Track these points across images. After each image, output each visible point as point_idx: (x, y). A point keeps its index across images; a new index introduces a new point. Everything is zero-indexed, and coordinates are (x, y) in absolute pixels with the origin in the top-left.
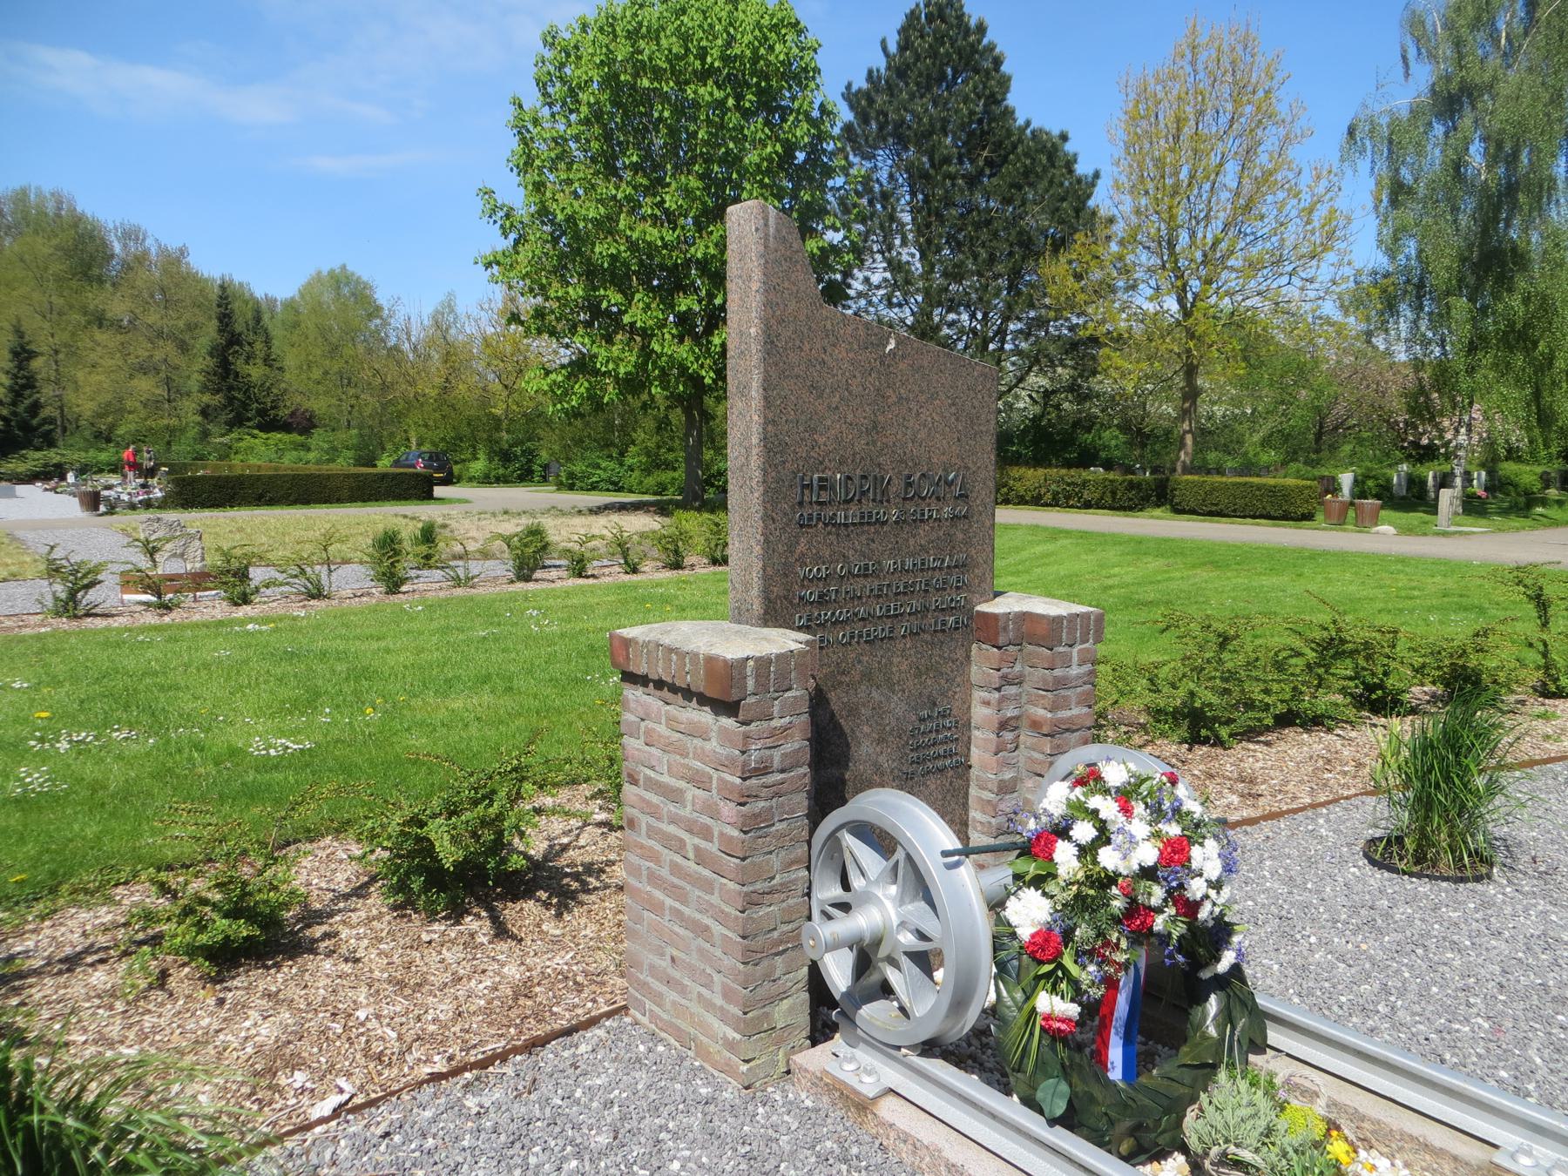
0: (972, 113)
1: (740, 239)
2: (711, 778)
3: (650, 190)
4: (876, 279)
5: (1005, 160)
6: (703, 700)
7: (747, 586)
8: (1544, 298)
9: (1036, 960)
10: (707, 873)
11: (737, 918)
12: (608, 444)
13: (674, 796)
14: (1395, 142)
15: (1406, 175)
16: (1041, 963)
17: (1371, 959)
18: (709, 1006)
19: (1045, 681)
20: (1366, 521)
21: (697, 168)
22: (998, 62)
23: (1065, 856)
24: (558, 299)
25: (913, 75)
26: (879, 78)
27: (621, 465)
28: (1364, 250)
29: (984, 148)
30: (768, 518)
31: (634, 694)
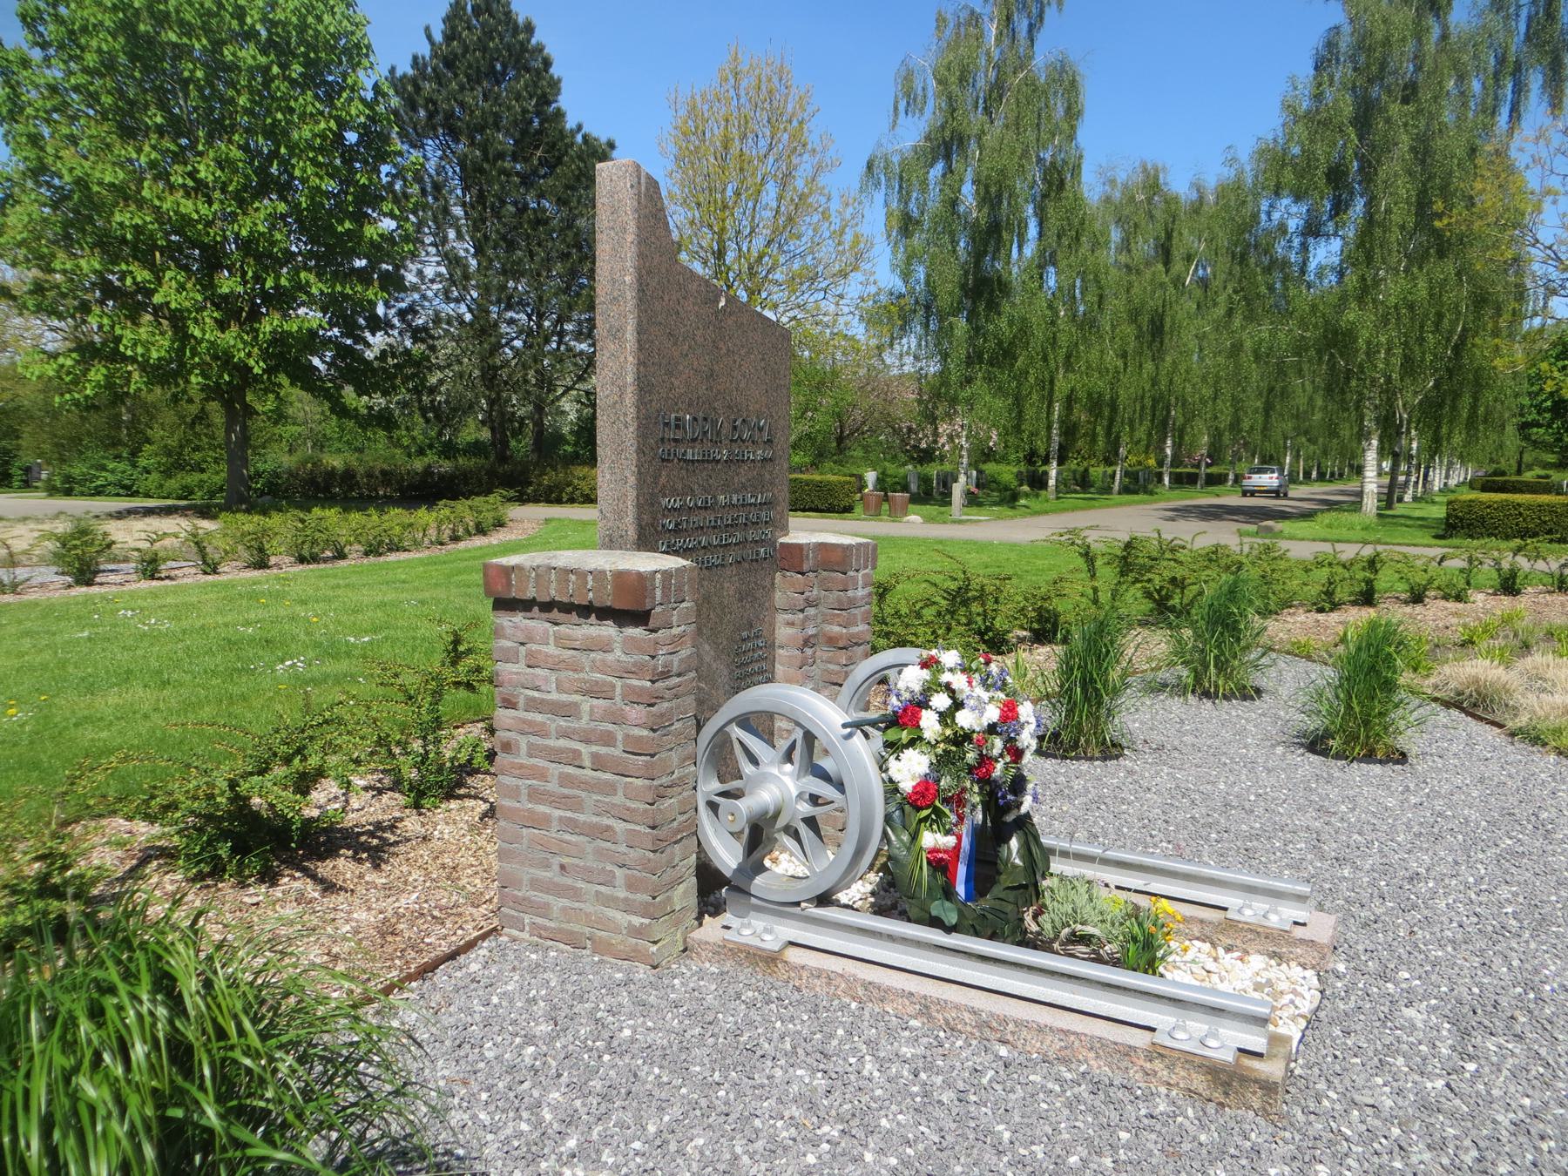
0: (525, 111)
1: (611, 194)
2: (614, 686)
3: (179, 157)
4: (429, 272)
5: (559, 161)
6: (605, 613)
7: (620, 515)
8: (1023, 319)
9: (918, 805)
10: (608, 776)
11: (646, 811)
12: (116, 443)
13: (568, 711)
14: (904, 180)
15: (913, 207)
16: (919, 809)
17: (1072, 815)
18: (609, 901)
19: (839, 600)
20: (897, 513)
21: (236, 137)
22: (547, 63)
23: (929, 723)
24: (64, 272)
25: (461, 66)
26: (425, 65)
27: (134, 466)
28: (882, 273)
29: (537, 148)
30: (640, 451)
31: (516, 622)
